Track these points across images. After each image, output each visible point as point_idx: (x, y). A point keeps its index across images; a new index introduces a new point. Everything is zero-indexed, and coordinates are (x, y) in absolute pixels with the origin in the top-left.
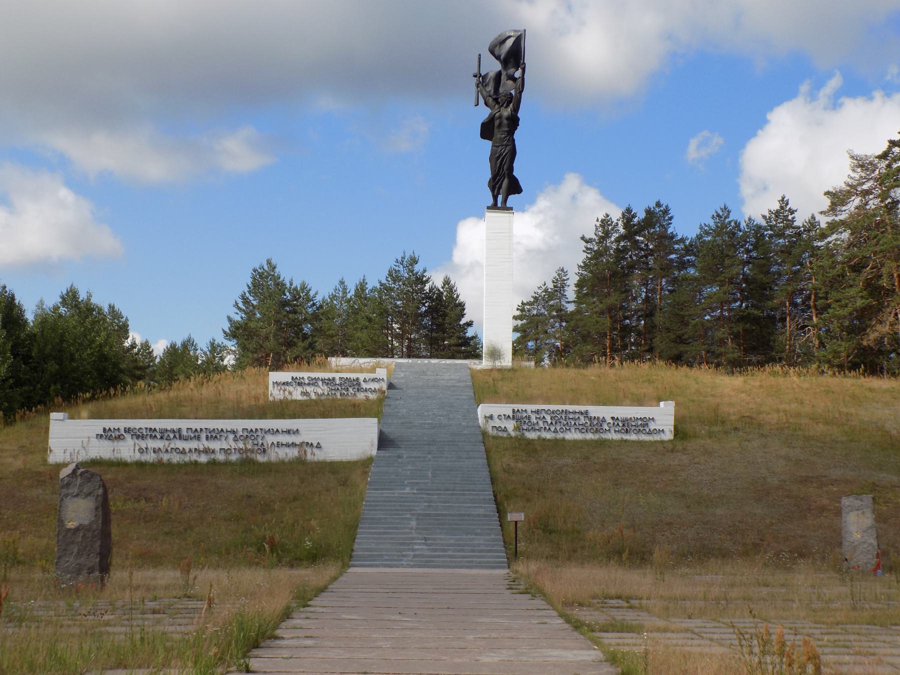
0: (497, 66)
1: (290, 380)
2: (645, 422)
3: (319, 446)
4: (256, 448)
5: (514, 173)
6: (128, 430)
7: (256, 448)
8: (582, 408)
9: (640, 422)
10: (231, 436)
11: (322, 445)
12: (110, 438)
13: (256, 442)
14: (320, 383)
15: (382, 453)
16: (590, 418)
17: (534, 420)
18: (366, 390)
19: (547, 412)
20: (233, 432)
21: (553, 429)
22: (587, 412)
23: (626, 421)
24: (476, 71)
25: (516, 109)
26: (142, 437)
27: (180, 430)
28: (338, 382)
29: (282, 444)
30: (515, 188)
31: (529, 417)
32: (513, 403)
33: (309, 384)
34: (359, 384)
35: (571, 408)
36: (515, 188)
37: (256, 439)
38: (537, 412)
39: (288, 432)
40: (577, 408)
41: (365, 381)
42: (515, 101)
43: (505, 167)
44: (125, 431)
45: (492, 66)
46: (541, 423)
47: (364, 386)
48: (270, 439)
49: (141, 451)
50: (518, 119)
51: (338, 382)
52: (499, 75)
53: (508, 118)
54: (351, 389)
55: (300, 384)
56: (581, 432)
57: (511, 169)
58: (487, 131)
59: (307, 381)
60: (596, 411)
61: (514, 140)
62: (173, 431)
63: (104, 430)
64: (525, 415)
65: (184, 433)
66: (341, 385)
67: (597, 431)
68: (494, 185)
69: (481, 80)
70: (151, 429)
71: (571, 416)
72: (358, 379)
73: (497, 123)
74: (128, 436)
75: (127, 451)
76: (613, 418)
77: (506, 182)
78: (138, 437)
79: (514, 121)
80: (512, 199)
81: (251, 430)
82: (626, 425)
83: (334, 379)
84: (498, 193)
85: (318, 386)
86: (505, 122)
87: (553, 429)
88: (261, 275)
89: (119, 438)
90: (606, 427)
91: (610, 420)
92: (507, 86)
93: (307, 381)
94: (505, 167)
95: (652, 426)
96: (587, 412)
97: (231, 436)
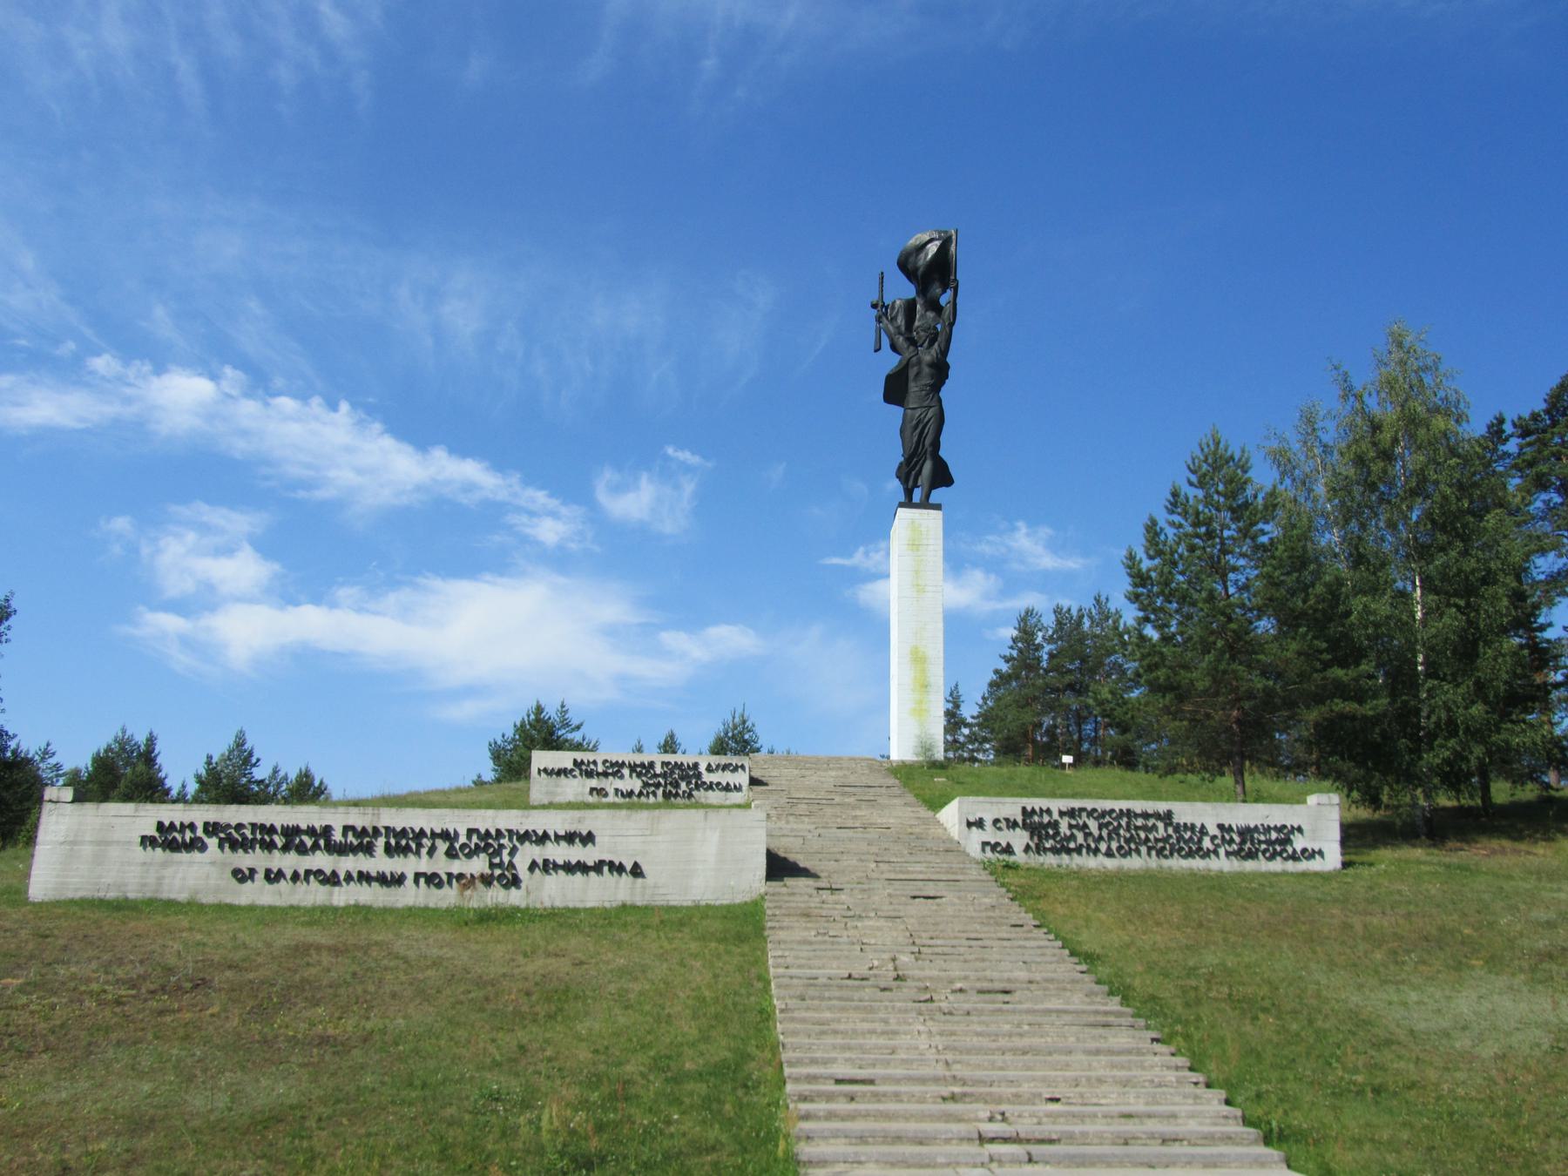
0: (908, 290)
1: (570, 765)
2: (1286, 834)
3: (637, 871)
4: (498, 872)
5: (941, 453)
6: (212, 828)
7: (498, 872)
8: (1162, 807)
9: (1274, 835)
10: (442, 846)
11: (645, 868)
12: (173, 846)
13: (497, 860)
14: (626, 771)
15: (775, 886)
16: (1177, 828)
17: (1064, 828)
18: (710, 787)
19: (1091, 813)
20: (445, 835)
21: (1103, 847)
22: (1169, 814)
23: (1246, 833)
24: (875, 298)
25: (945, 352)
26: (245, 845)
27: (327, 830)
29: (556, 867)
30: (942, 477)
31: (1055, 825)
32: (1021, 796)
33: (605, 774)
34: (699, 776)
35: (1138, 806)
36: (942, 477)
37: (498, 852)
38: (1071, 813)
39: (570, 838)
41: (709, 769)
42: (941, 339)
43: (928, 442)
44: (206, 831)
45: (901, 290)
47: (708, 778)
48: (527, 854)
49: (242, 876)
50: (947, 367)
52: (910, 307)
53: (931, 365)
54: (683, 785)
55: (589, 774)
56: (1160, 853)
57: (936, 445)
58: (895, 389)
60: (1188, 812)
61: (940, 401)
62: (311, 831)
63: (160, 826)
64: (1046, 819)
65: (337, 836)
66: (664, 775)
67: (1190, 854)
68: (908, 474)
69: (882, 309)
70: (263, 827)
71: (1140, 822)
72: (696, 765)
73: (912, 372)
74: (212, 842)
75: (258, 893)
76: (1221, 827)
77: (927, 467)
78: (234, 845)
79: (941, 371)
80: (938, 495)
81: (488, 832)
82: (1247, 842)
84: (916, 485)
85: (622, 777)
86: (926, 370)
87: (1103, 847)
89: (196, 845)
91: (1213, 830)
92: (923, 317)
94: (928, 442)
95: (1299, 843)
96: (1169, 814)
97: (442, 846)
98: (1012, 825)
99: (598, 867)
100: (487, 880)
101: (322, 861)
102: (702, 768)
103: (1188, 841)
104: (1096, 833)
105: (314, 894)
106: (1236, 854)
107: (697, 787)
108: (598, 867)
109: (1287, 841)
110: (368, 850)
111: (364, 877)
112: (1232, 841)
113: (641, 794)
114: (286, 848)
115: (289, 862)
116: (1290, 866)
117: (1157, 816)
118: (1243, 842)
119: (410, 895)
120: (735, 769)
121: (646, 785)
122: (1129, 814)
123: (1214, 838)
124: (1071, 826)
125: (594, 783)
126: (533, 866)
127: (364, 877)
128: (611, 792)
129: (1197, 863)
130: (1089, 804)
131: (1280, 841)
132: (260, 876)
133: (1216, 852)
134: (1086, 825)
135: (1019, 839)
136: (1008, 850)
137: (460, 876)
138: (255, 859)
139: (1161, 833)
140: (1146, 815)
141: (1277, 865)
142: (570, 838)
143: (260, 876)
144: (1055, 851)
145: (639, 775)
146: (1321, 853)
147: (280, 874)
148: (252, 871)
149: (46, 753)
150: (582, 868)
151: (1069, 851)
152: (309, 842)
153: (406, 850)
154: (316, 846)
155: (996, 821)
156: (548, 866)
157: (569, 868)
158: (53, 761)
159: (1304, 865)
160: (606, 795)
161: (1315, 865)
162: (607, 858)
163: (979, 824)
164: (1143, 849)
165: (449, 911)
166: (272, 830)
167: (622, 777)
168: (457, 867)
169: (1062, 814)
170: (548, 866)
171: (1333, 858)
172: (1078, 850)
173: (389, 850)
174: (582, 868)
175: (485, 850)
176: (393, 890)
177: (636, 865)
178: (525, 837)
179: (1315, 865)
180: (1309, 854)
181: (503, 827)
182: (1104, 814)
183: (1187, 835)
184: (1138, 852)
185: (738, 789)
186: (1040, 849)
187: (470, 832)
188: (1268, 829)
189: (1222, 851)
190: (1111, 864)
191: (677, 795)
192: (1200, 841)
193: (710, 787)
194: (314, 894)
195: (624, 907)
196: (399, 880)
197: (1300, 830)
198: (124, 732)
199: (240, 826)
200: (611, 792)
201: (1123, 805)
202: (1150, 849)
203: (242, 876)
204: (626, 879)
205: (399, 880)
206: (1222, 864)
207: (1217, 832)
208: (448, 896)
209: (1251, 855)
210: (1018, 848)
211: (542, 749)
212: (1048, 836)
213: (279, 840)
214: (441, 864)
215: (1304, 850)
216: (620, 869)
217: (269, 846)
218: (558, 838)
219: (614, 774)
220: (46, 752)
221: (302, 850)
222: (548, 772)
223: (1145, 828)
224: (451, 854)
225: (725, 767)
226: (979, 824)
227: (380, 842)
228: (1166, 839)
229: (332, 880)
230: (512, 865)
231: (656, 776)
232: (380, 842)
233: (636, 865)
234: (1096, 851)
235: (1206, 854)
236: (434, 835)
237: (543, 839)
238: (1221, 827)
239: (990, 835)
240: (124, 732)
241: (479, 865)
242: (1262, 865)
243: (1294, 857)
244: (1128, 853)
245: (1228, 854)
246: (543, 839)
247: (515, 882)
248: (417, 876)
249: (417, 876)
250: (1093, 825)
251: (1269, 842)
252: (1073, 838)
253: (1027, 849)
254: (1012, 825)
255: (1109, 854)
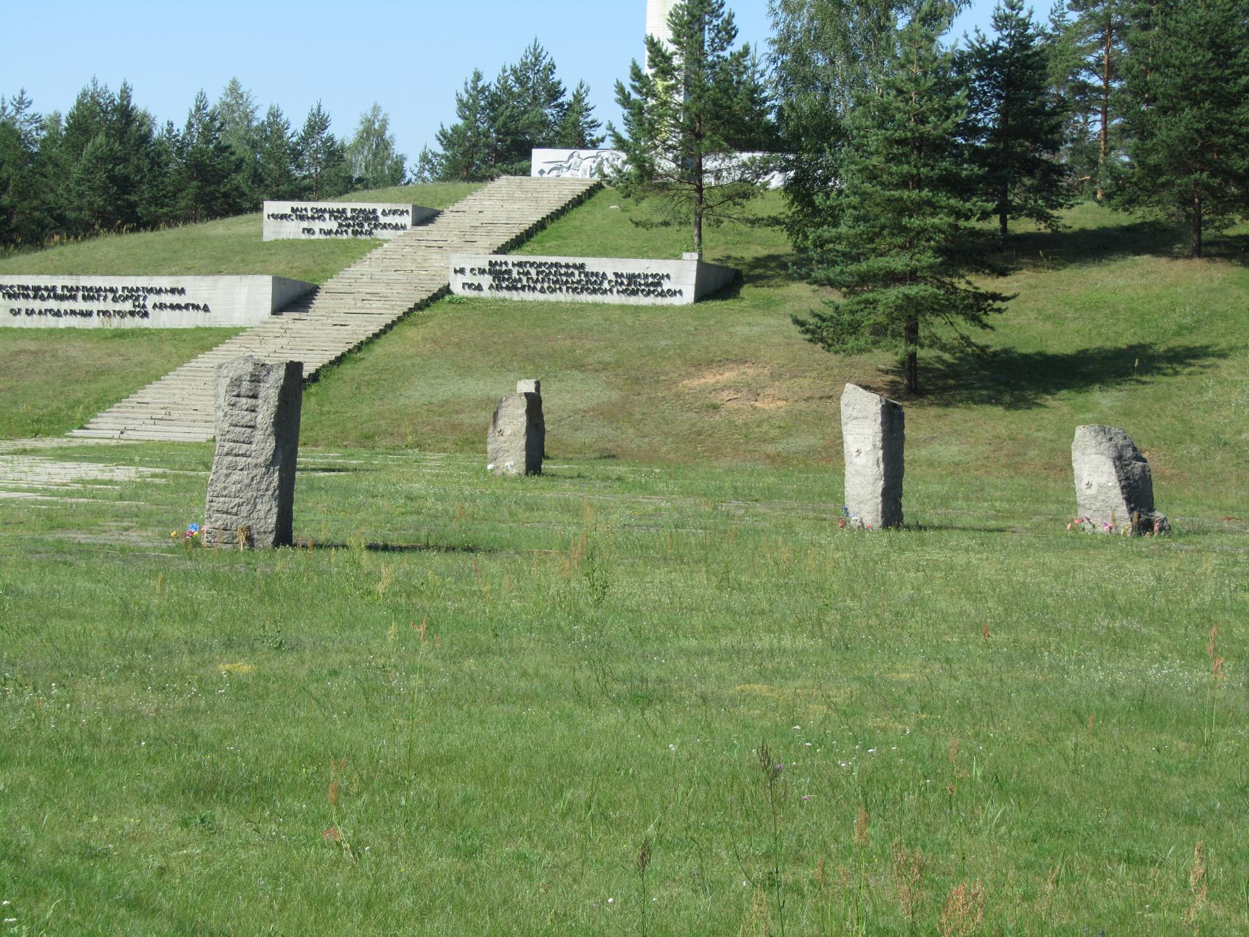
1: (289, 212)
2: (658, 280)
3: (206, 309)
9: (650, 280)
10: (110, 296)
14: (327, 216)
16: (586, 275)
17: (515, 275)
18: (384, 226)
19: (532, 265)
20: (111, 290)
22: (582, 266)
23: (632, 278)
27: (54, 288)
28: (349, 215)
29: (166, 306)
31: (509, 272)
33: (313, 218)
34: (376, 218)
35: (563, 260)
37: (137, 298)
38: (520, 264)
39: (173, 291)
40: (571, 260)
41: (384, 213)
46: (524, 279)
47: (382, 220)
48: (152, 299)
49: (15, 312)
51: (349, 215)
54: (366, 225)
55: (302, 218)
56: (574, 290)
59: (310, 214)
60: (594, 264)
62: (46, 289)
64: (504, 268)
65: (59, 291)
66: (353, 218)
67: (594, 291)
72: (374, 211)
75: (22, 322)
76: (616, 274)
78: (10, 296)
82: (631, 284)
83: (344, 211)
85: (324, 220)
87: (539, 286)
88: (93, 114)
90: (606, 285)
91: (611, 277)
93: (310, 214)
95: (666, 285)
96: (582, 266)
97: (110, 296)
98: (482, 272)
99: (187, 307)
100: (132, 313)
101: (52, 304)
102: (379, 213)
103: (593, 283)
104: (535, 277)
105: (50, 322)
106: (624, 292)
107: (376, 226)
108: (187, 307)
109: (659, 284)
110: (74, 298)
111: (73, 313)
112: (622, 283)
113: (337, 232)
114: (35, 297)
115: (37, 305)
116: (660, 301)
117: (575, 266)
118: (629, 284)
119: (95, 322)
120: (402, 213)
121: (340, 225)
122: (557, 265)
123: (610, 282)
124: (519, 273)
125: (306, 224)
126: (155, 306)
127: (73, 313)
128: (317, 231)
129: (598, 298)
130: (532, 259)
131: (654, 284)
132: (23, 312)
133: (611, 290)
134: (528, 273)
135: (486, 280)
136: (479, 288)
137: (119, 312)
138: (20, 303)
139: (577, 278)
140: (567, 266)
141: (650, 300)
142: (173, 291)
143: (23, 312)
144: (508, 288)
145: (336, 218)
146: (680, 292)
147: (33, 311)
148: (20, 310)
149: (21, 103)
150: (178, 307)
151: (516, 289)
152: (46, 294)
153: (92, 298)
154: (49, 296)
155: (472, 270)
156: (162, 306)
157: (172, 307)
158: (29, 111)
159: (668, 301)
160: (314, 233)
161: (676, 301)
162: (191, 302)
163: (462, 271)
164: (564, 288)
165: (96, 330)
166: (27, 288)
167: (324, 220)
168: (120, 306)
169: (514, 265)
170: (162, 306)
171: (689, 296)
172: (523, 288)
173: (84, 298)
174: (178, 307)
175: (131, 297)
176: (88, 319)
177: (205, 306)
178: (151, 291)
179: (676, 301)
180: (672, 293)
181: (140, 286)
182: (540, 265)
183: (593, 279)
184: (560, 289)
185: (404, 227)
186: (499, 288)
187: (123, 289)
188: (646, 276)
189: (615, 290)
190: (541, 297)
191: (361, 233)
192: (601, 283)
193: (384, 226)
194: (50, 322)
195: (198, 329)
196: (89, 314)
197: (668, 276)
198: (95, 84)
199: (12, 287)
200: (317, 231)
201: (554, 259)
202: (568, 289)
203: (15, 312)
204: (201, 313)
205: (89, 314)
206: (614, 299)
207: (613, 278)
208: (116, 322)
209: (634, 293)
210: (485, 287)
211: (272, 199)
212: (504, 279)
213: (31, 293)
214: (110, 306)
215: (669, 291)
216: (196, 307)
217: (27, 297)
218: (166, 291)
219: (319, 218)
220: (21, 102)
221: (43, 298)
222: (274, 216)
223: (566, 274)
224: (115, 300)
225: (395, 212)
226: (462, 271)
227: (80, 294)
228: (579, 282)
229: (57, 314)
230: (144, 306)
231: (346, 219)
232: (80, 294)
233: (205, 306)
234: (534, 289)
235: (605, 292)
236: (106, 290)
237: (159, 291)
238: (616, 274)
239: (468, 278)
240: (95, 84)
241: (128, 306)
242: (641, 300)
243: (662, 294)
244: (554, 291)
245: (618, 292)
246: (159, 291)
247: (146, 314)
248: (98, 312)
249: (98, 312)
250: (533, 272)
251: (647, 285)
252: (520, 280)
253: (491, 287)
254: (482, 272)
255: (542, 291)
